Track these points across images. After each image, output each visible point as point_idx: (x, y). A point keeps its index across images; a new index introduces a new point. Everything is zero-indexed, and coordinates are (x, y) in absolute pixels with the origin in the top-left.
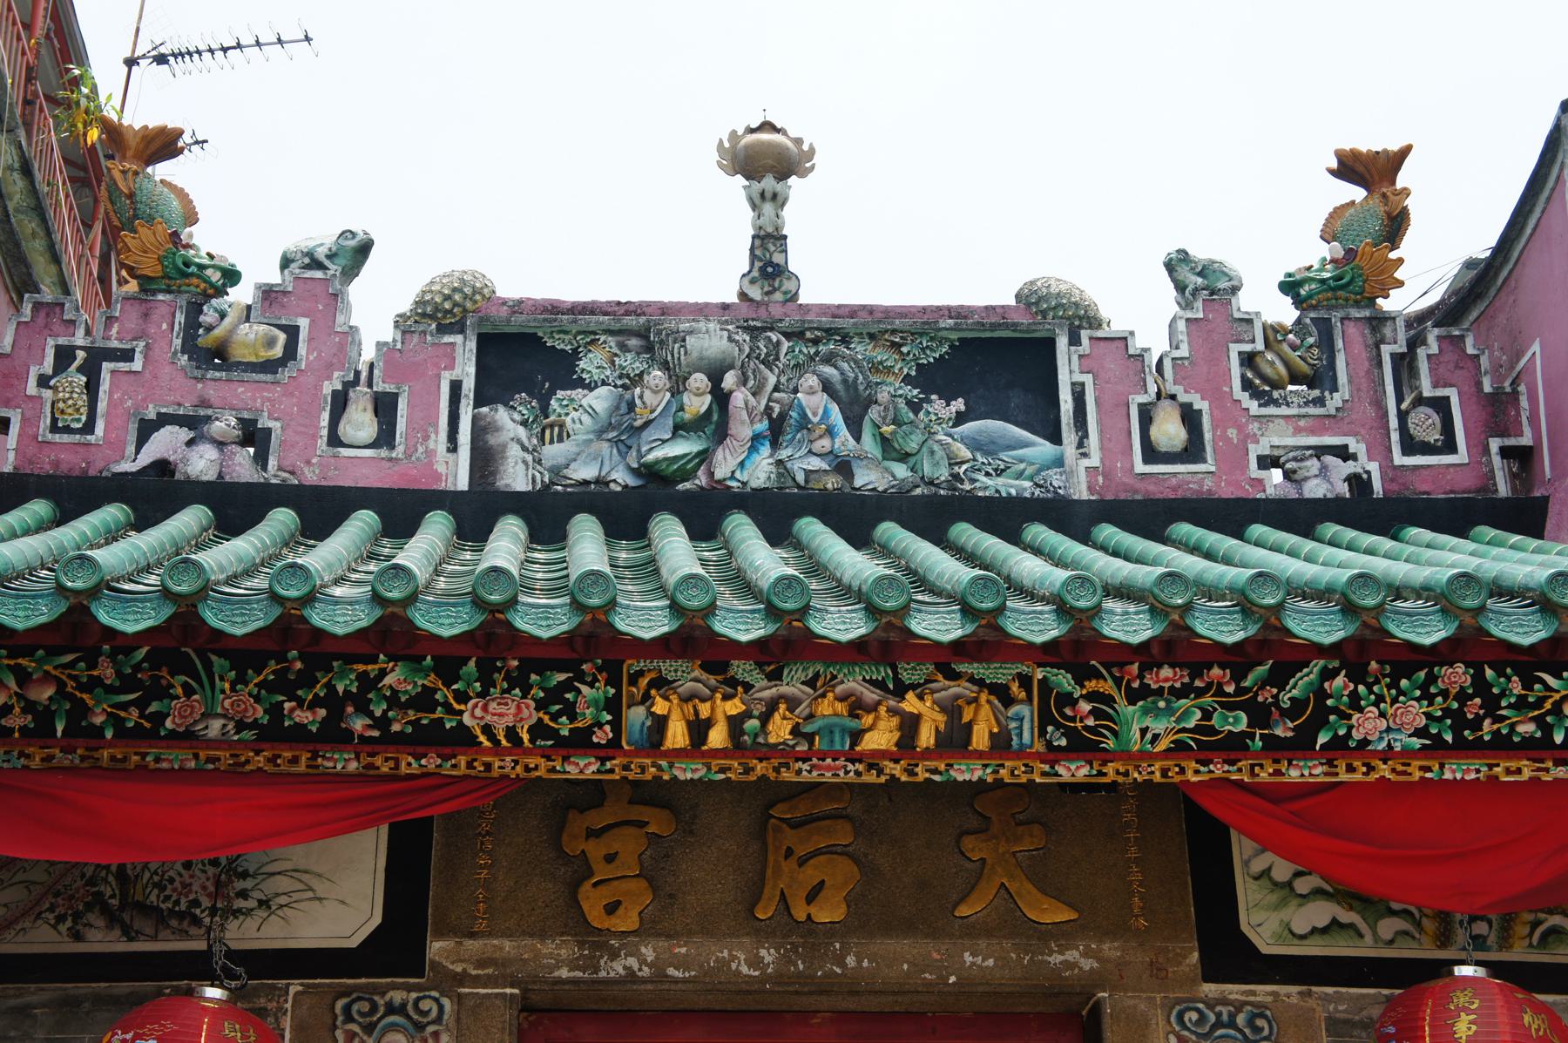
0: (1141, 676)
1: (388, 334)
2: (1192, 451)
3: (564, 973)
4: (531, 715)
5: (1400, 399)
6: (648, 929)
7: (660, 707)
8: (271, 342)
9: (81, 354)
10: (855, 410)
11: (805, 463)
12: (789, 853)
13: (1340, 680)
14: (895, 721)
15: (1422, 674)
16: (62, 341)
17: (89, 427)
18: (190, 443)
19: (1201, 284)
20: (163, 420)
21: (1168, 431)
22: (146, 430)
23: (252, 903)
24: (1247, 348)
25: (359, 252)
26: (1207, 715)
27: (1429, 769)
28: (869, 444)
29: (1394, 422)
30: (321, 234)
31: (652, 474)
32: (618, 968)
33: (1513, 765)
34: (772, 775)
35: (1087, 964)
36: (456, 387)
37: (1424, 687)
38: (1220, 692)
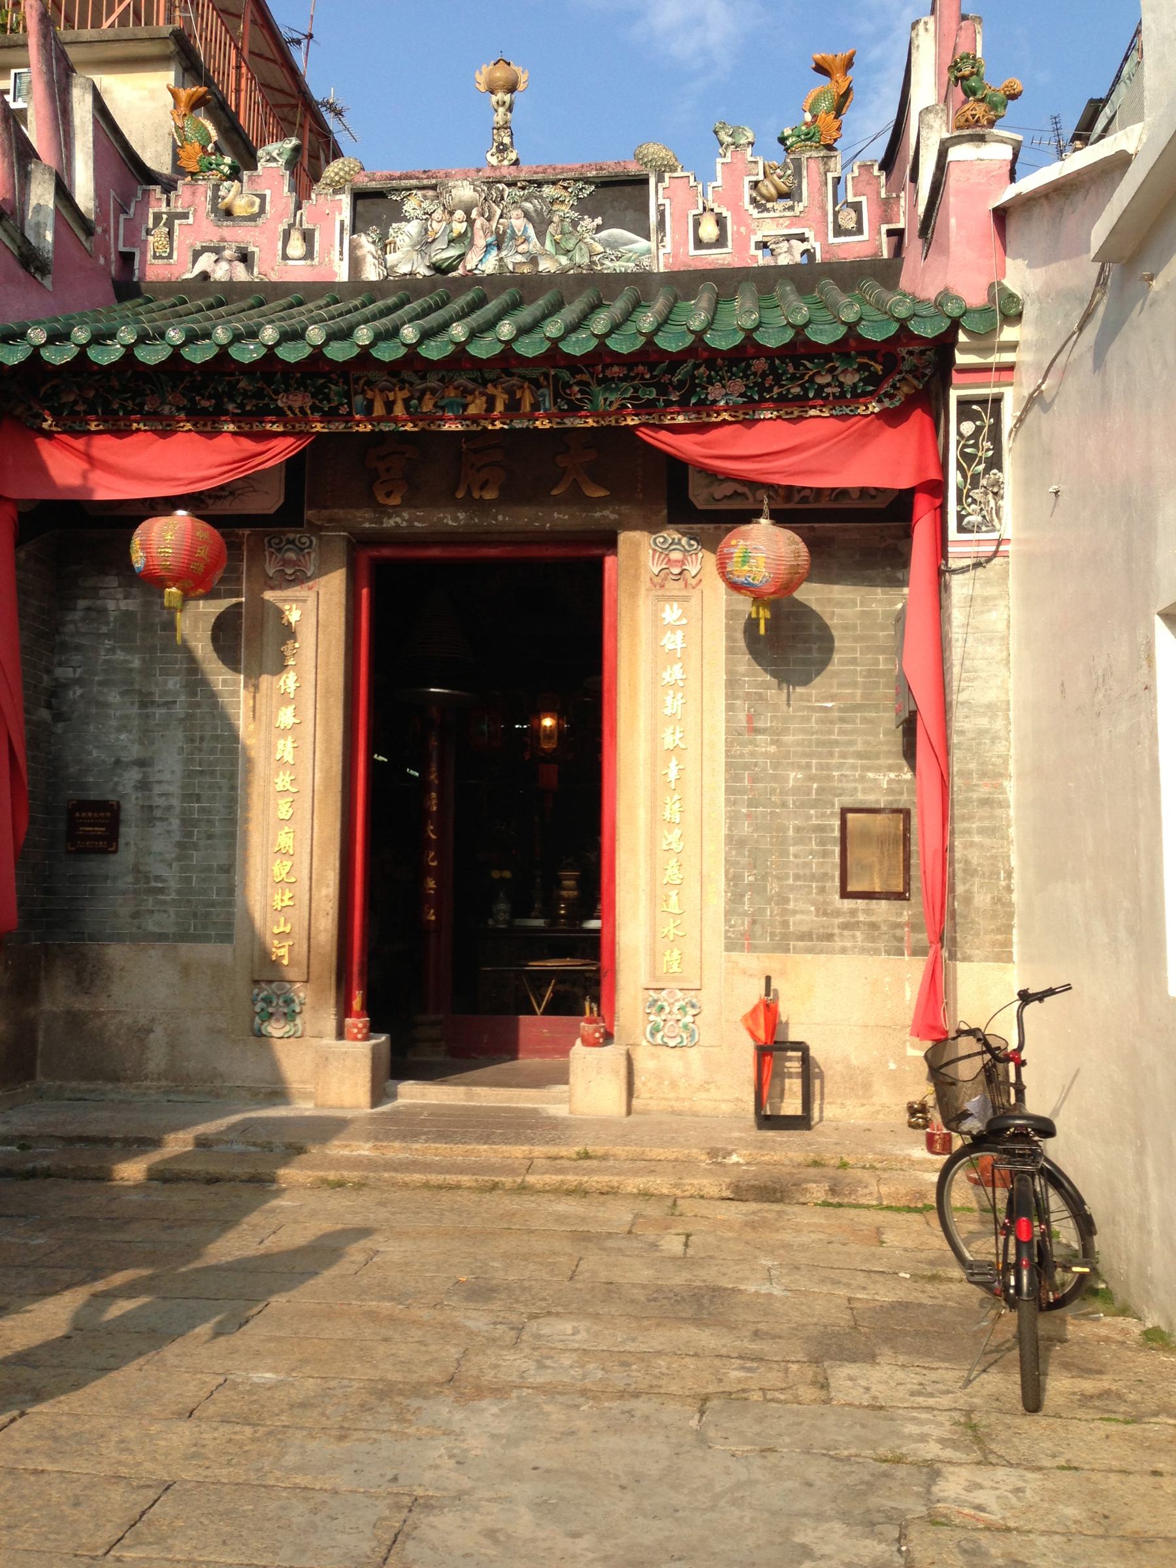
0: (603, 371)
2: (720, 242)
3: (367, 525)
5: (835, 203)
6: (407, 503)
7: (370, 395)
8: (252, 204)
9: (165, 216)
10: (541, 223)
12: (473, 465)
13: (702, 369)
14: (484, 399)
15: (744, 364)
16: (156, 210)
17: (170, 256)
18: (216, 261)
20: (205, 249)
21: (709, 230)
22: (197, 255)
23: (226, 493)
24: (754, 178)
26: (636, 391)
27: (747, 414)
28: (549, 246)
29: (831, 218)
32: (392, 522)
33: (789, 410)
34: (427, 428)
35: (613, 517)
36: (342, 223)
37: (744, 371)
38: (643, 378)
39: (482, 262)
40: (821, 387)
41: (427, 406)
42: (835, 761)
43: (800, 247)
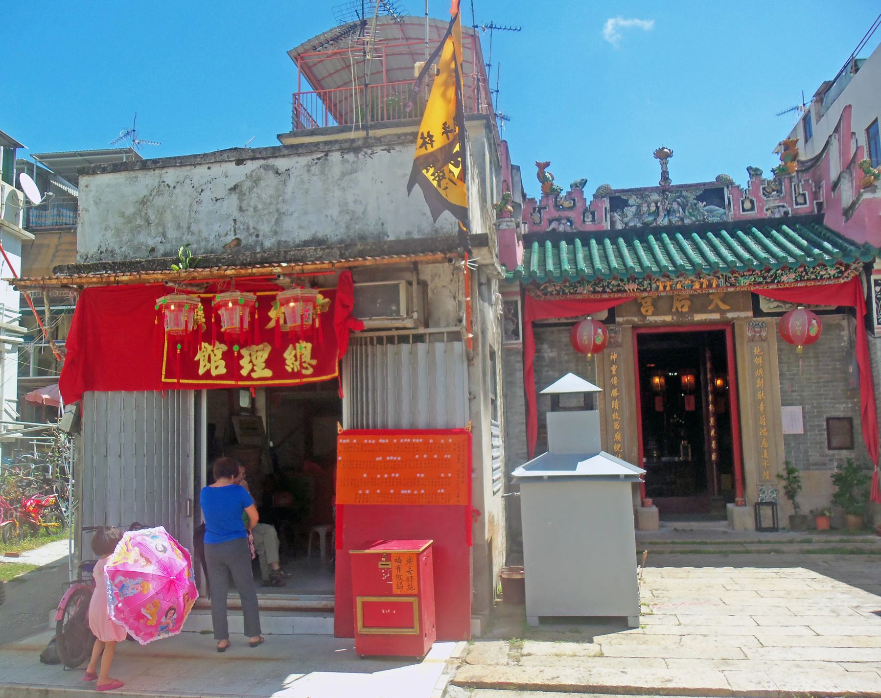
1: (592, 199)
2: (752, 209)
4: (636, 286)
11: (675, 220)
19: (754, 173)
20: (553, 220)
21: (747, 205)
22: (550, 222)
25: (584, 183)
30: (578, 179)
31: (646, 225)
39: (663, 221)
40: (822, 276)
41: (679, 286)
42: (823, 401)
43: (782, 210)
